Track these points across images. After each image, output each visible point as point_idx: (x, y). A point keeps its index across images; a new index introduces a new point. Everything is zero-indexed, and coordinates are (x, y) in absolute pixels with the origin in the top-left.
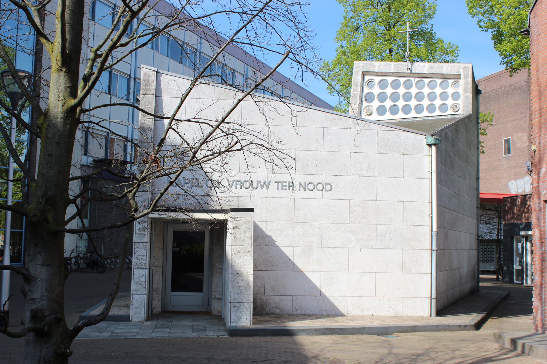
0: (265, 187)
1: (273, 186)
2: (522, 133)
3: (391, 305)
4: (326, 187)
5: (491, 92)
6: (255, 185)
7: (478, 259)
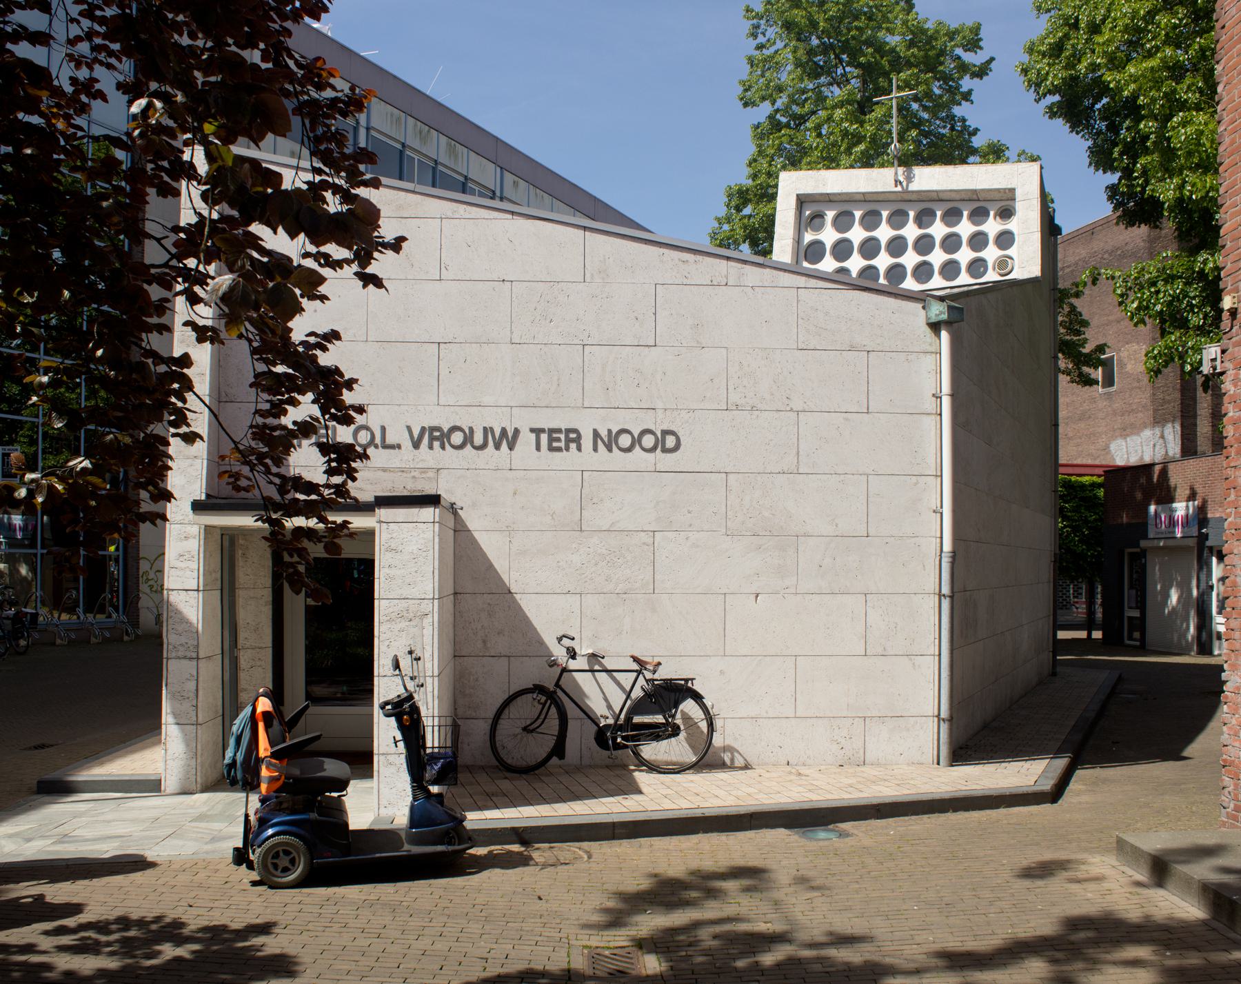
0: (504, 445)
1: (527, 439)
2: (1138, 343)
3: (835, 738)
4: (667, 442)
5: (1076, 264)
6: (478, 439)
7: (1055, 601)
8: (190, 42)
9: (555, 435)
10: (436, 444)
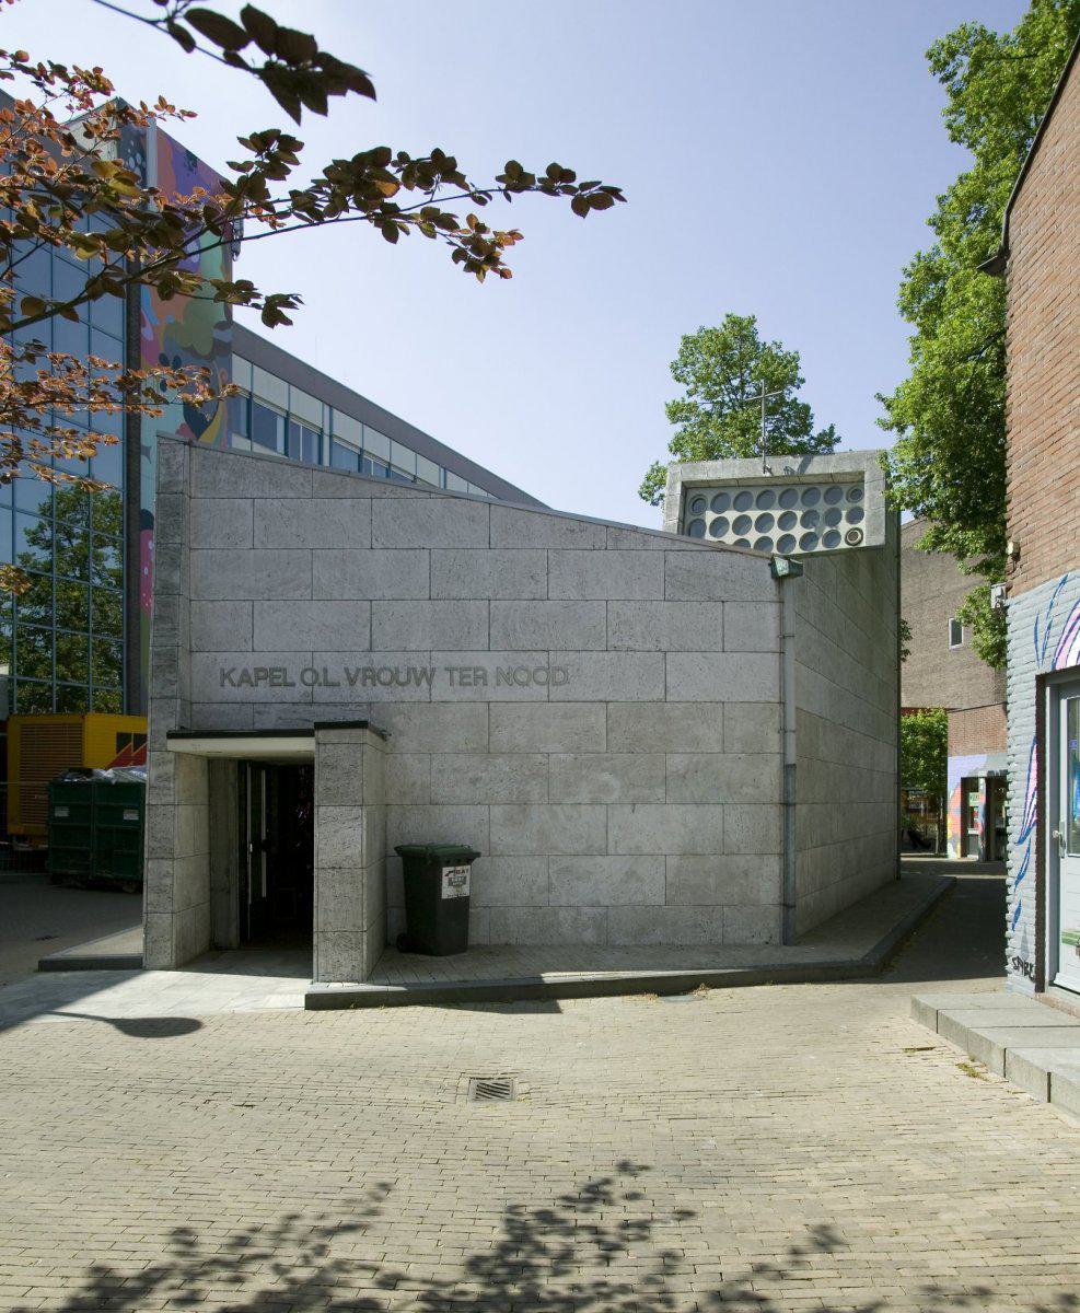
6: (403, 677)
8: (708, 523)
9: (465, 673)
10: (369, 681)
